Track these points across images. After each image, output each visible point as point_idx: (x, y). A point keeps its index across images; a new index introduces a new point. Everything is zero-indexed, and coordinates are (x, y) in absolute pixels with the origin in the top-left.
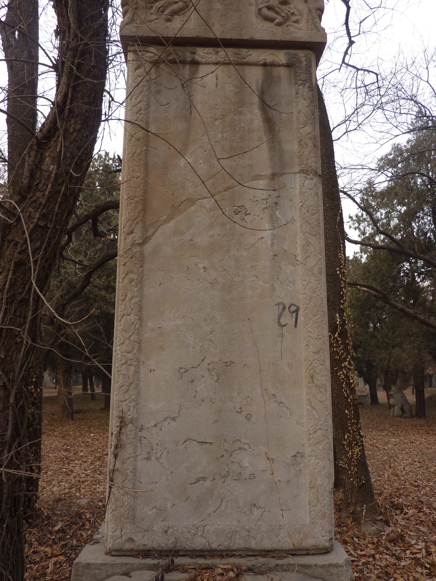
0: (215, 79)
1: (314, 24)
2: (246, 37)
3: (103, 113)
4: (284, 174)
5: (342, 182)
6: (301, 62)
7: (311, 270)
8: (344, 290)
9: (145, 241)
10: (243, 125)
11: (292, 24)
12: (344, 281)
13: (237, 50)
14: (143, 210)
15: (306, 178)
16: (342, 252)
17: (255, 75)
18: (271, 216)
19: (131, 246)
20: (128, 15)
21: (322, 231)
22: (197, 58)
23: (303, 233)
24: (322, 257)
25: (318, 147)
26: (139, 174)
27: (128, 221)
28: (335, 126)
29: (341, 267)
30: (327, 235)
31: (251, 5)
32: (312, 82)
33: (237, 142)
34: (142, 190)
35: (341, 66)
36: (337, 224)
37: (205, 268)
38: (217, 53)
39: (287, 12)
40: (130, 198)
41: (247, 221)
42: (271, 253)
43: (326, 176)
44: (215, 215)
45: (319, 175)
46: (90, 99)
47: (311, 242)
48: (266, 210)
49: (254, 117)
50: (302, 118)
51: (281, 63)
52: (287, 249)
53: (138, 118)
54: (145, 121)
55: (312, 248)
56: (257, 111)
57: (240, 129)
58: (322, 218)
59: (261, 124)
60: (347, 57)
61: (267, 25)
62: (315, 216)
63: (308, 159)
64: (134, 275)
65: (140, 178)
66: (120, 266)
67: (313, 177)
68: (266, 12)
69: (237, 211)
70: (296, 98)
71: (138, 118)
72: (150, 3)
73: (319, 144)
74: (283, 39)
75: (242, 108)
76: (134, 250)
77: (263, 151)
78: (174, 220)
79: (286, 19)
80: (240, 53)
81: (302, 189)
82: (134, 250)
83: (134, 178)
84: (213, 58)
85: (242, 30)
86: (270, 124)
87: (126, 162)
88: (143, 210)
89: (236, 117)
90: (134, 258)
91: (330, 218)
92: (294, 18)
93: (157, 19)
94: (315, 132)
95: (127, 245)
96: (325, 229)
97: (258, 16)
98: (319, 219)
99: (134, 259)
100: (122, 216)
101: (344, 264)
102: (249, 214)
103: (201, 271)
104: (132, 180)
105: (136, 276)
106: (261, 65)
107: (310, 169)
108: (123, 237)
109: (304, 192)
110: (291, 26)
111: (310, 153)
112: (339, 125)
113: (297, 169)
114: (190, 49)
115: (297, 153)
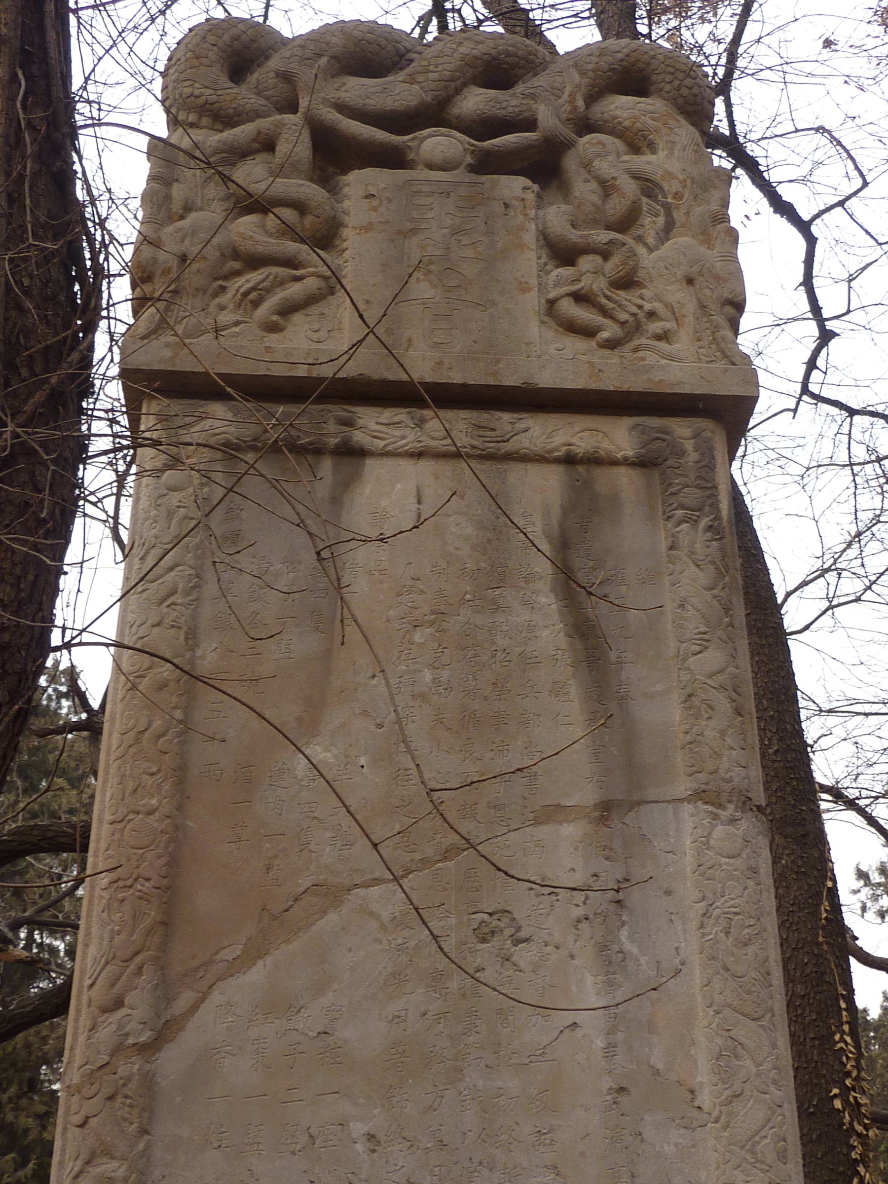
0: (413, 500)
1: (718, 344)
2: (510, 381)
3: (59, 622)
4: (639, 803)
5: (825, 768)
6: (683, 453)
7: (748, 1147)
8: (861, 1169)
9: (164, 1033)
10: (502, 642)
11: (649, 342)
12: (859, 1135)
13: (483, 417)
14: (162, 923)
15: (716, 817)
16: (846, 1028)
17: (539, 493)
18: (603, 948)
19: (112, 1055)
20: (150, 312)
21: (779, 1002)
22: (360, 437)
23: (715, 1007)
24: (785, 1095)
25: (750, 713)
26: (154, 802)
27: (107, 963)
28: (791, 588)
29: (848, 1082)
30: (791, 966)
31: (524, 289)
32: (719, 511)
33: (486, 698)
34: (160, 856)
35: (800, 400)
36: (823, 928)
37: (373, 1136)
38: (421, 423)
39: (635, 310)
40: (121, 884)
41: (522, 964)
42: (607, 1083)
43: (774, 761)
44: (413, 943)
45: (759, 808)
46: (19, 590)
47: (743, 1040)
48: (585, 925)
49: (538, 618)
50: (694, 624)
51: (618, 456)
52: (660, 1066)
53: (163, 618)
54: (185, 628)
55: (748, 1063)
56: (547, 601)
57: (493, 657)
58: (774, 954)
59: (563, 641)
60: (816, 376)
61: (575, 344)
62: (751, 949)
63: (718, 755)
64: (115, 1164)
65: (157, 814)
66: (65, 1129)
67: (738, 814)
68: (568, 307)
69: (487, 930)
70: (671, 560)
71: (163, 618)
72: (216, 279)
73: (750, 705)
74: (625, 388)
75: (498, 592)
76: (123, 1070)
77: (571, 728)
78: (269, 960)
79: (632, 329)
80: (492, 426)
81: (701, 854)
82: (123, 1070)
83: (138, 813)
84: (410, 438)
85: (498, 361)
86: (590, 643)
87: (112, 758)
88: (162, 923)
89: (479, 620)
90: (120, 1098)
91: (796, 908)
92: (656, 327)
93: (237, 323)
94: (737, 668)
95: (99, 1052)
96: (782, 945)
97: (546, 319)
98: (766, 960)
99: (117, 1104)
100: (86, 946)
101: (854, 1074)
102: (526, 940)
103: (359, 1147)
104: (130, 821)
105: (122, 1170)
106: (558, 461)
107: (728, 787)
108: (85, 1022)
109: (709, 864)
110: (648, 348)
111: (723, 734)
112: (805, 583)
113: (683, 787)
114: (339, 410)
115: (681, 735)
